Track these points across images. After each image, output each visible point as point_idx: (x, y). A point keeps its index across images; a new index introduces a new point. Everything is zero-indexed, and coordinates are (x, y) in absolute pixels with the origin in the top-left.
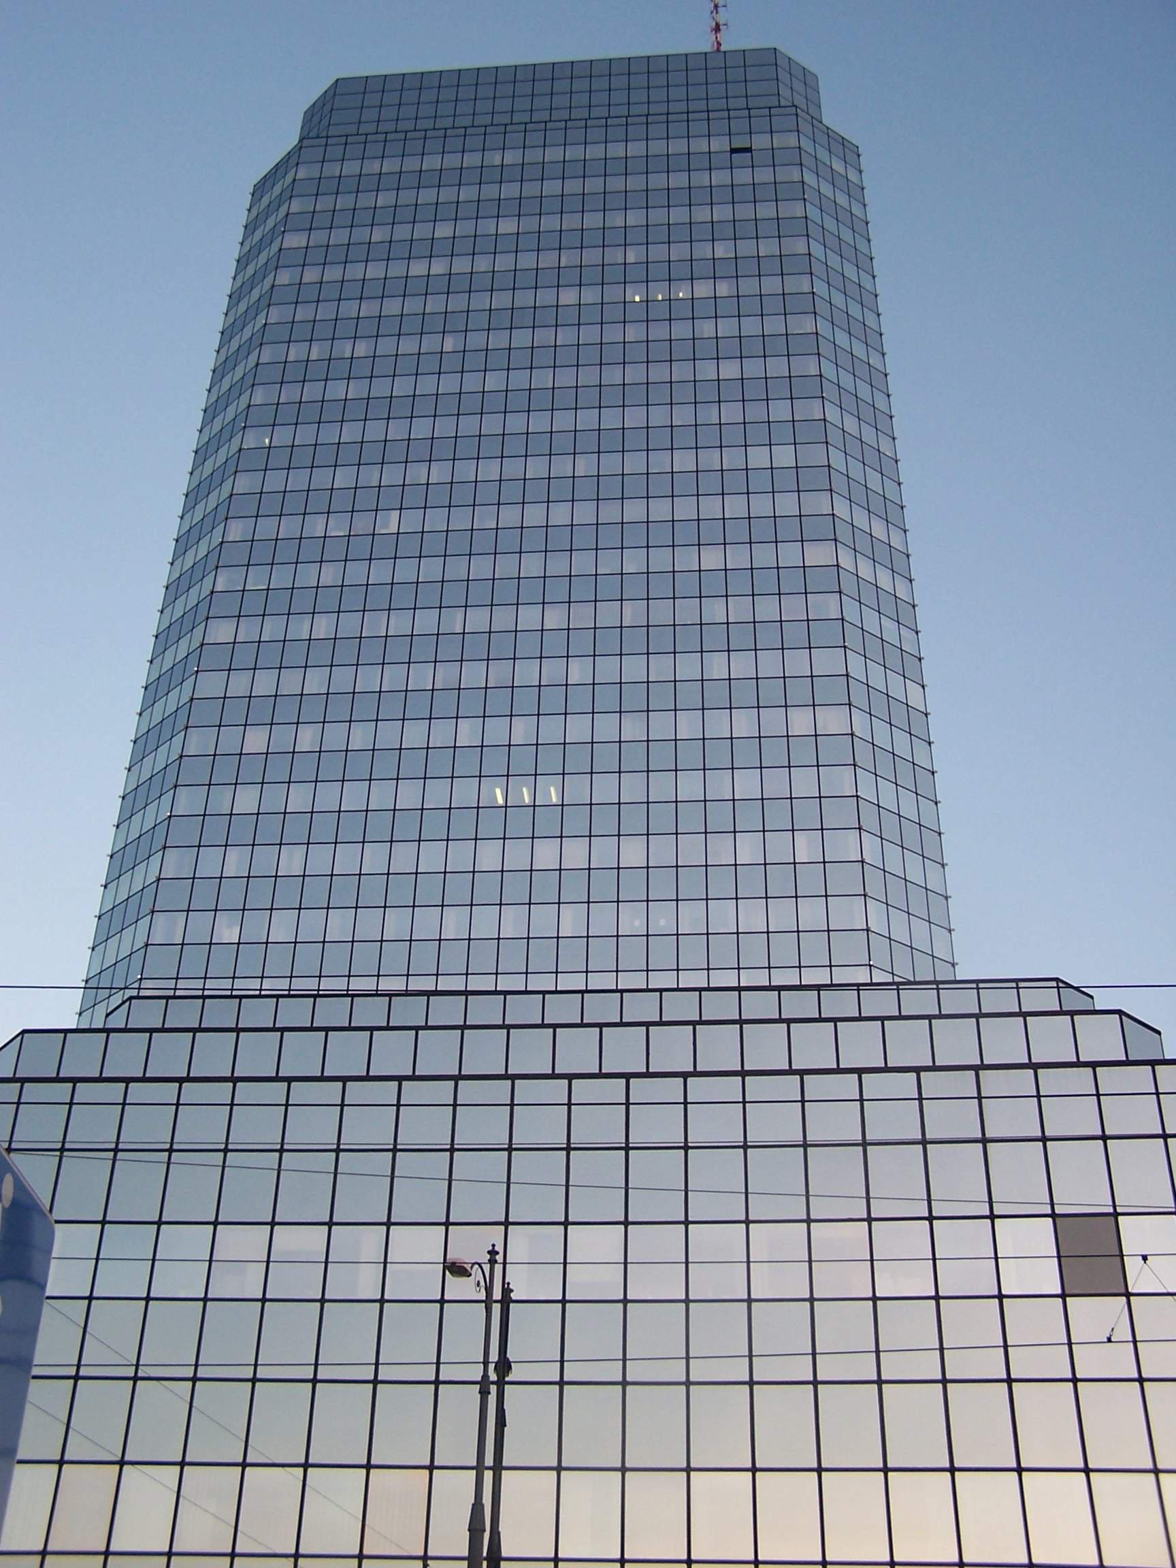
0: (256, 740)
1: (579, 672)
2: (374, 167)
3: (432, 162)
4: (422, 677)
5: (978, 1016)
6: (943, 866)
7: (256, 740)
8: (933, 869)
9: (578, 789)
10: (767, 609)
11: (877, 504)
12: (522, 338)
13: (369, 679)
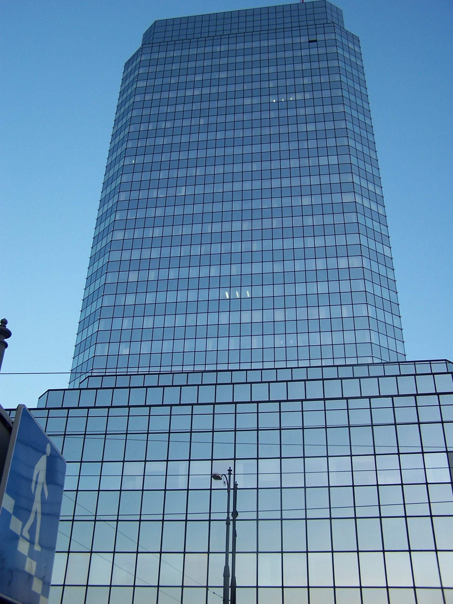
0: (133, 277)
1: (256, 246)
2: (171, 54)
3: (193, 51)
4: (196, 250)
5: (415, 375)
6: (400, 317)
7: (133, 277)
8: (396, 319)
9: (258, 291)
10: (328, 219)
11: (370, 177)
12: (230, 118)
13: (176, 252)
